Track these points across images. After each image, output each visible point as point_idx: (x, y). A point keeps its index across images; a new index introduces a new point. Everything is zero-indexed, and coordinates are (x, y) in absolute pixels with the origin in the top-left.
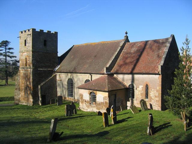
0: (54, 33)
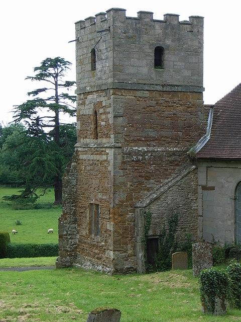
0: (188, 20)
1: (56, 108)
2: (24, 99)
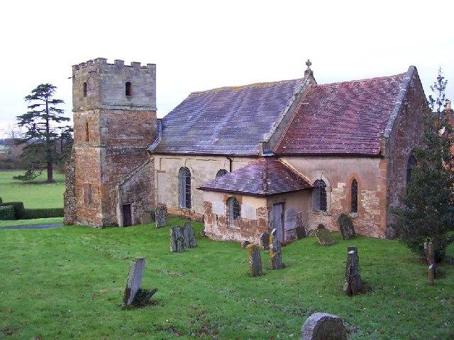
1: (46, 117)
2: (26, 111)
